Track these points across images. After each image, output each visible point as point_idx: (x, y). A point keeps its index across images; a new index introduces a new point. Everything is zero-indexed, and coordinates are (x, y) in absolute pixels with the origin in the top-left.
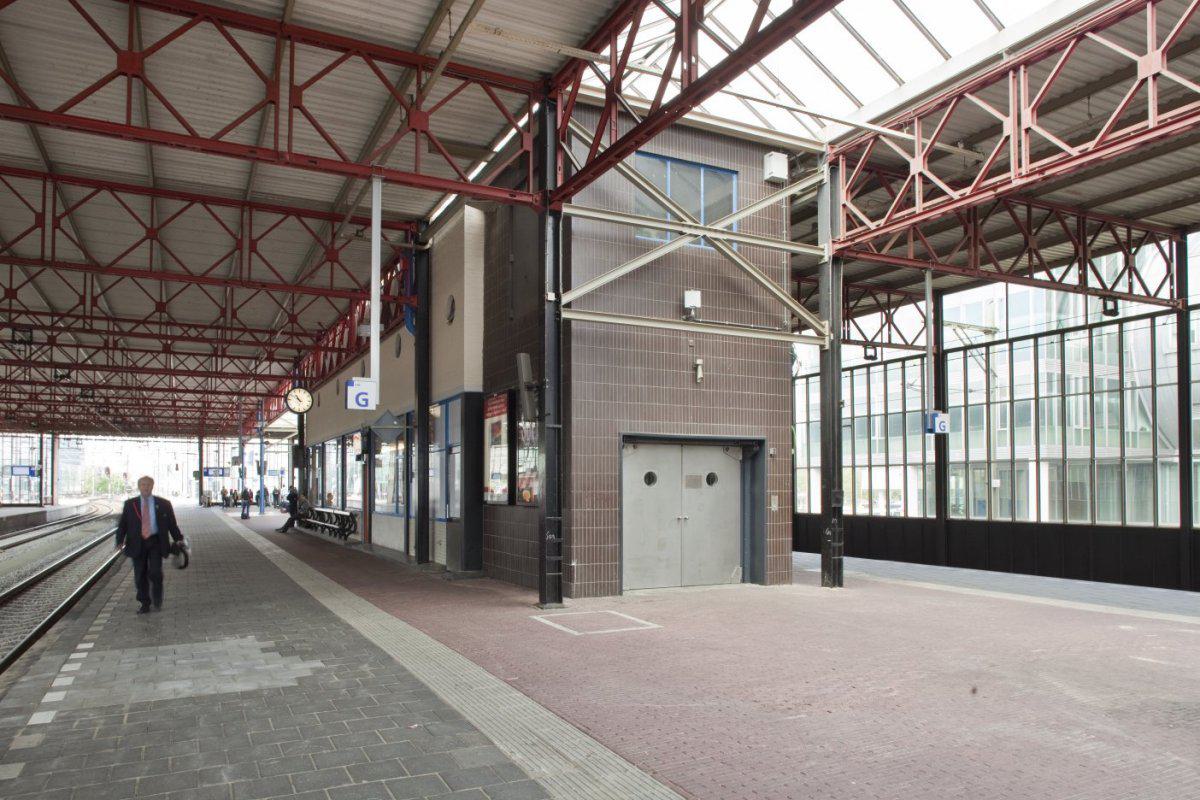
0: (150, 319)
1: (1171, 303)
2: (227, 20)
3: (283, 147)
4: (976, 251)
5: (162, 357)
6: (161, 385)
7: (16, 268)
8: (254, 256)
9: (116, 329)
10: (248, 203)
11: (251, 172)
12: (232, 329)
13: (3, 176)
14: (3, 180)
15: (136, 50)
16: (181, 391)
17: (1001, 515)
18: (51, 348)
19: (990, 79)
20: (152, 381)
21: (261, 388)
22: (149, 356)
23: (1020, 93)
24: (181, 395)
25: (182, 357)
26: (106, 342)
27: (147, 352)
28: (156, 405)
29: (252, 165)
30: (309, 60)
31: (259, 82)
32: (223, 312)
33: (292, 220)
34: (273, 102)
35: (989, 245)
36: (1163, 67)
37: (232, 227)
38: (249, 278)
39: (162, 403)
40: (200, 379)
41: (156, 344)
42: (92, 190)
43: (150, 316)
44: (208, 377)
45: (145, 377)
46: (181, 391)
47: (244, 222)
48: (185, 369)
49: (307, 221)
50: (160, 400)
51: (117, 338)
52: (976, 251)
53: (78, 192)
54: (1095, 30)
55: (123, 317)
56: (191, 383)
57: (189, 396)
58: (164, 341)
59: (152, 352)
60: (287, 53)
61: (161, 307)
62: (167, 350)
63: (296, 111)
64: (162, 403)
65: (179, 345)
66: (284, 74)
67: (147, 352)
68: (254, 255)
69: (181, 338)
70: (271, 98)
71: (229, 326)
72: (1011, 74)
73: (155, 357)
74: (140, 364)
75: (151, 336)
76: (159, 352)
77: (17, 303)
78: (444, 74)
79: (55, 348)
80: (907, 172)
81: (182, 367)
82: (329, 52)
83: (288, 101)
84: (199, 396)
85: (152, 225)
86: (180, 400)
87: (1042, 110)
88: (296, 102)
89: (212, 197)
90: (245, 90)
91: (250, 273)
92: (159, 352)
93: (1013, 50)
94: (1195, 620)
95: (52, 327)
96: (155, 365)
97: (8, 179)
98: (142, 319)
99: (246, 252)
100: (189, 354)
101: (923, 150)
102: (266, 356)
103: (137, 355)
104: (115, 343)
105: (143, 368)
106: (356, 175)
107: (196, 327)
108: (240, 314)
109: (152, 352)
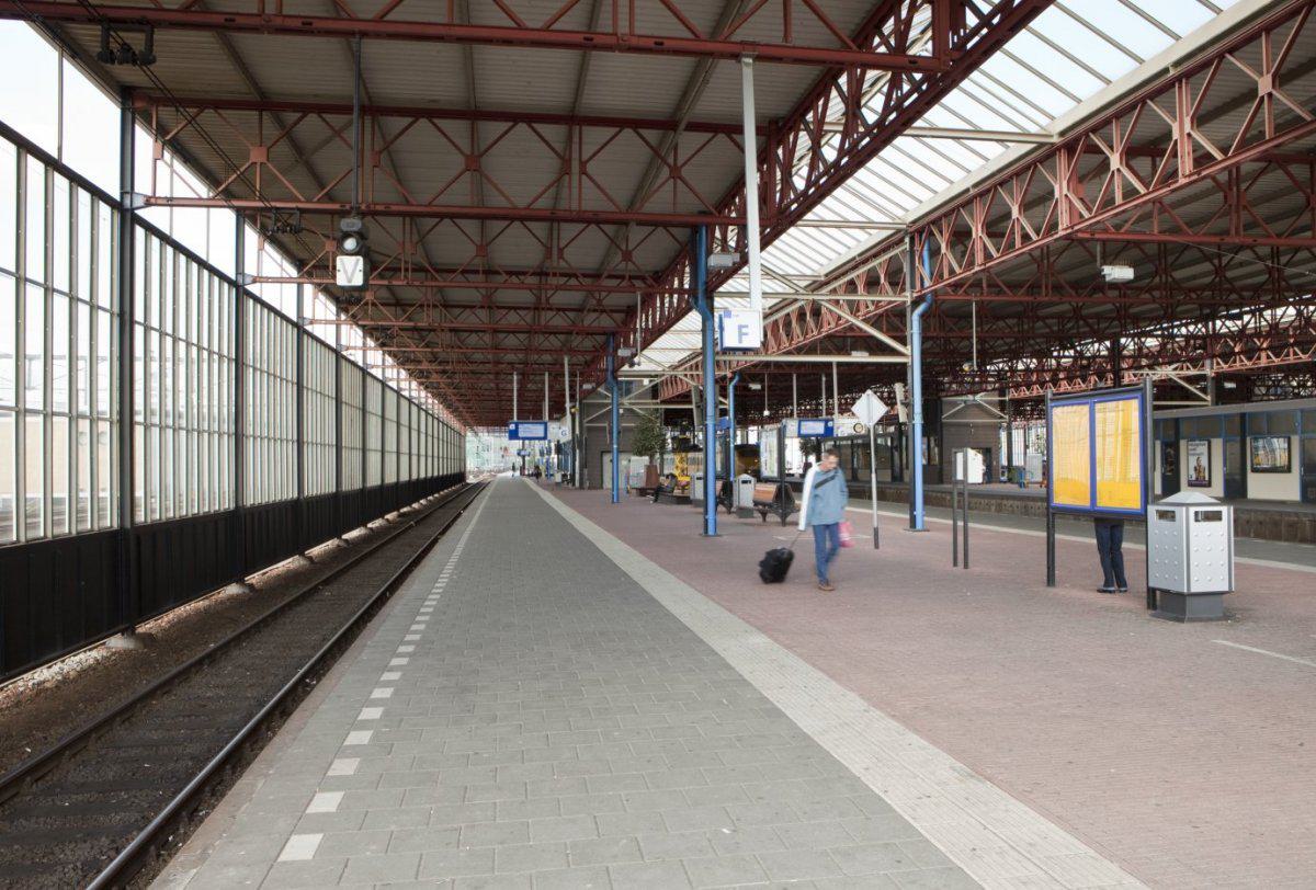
3: (623, 28)
4: (1239, 217)
7: (266, 116)
10: (573, 118)
11: (556, 198)
15: (476, 153)
19: (1158, 88)
21: (588, 343)
23: (1185, 102)
29: (584, 57)
31: (541, 247)
32: (548, 251)
33: (628, 133)
35: (1254, 210)
36: (1121, 163)
37: (559, 147)
47: (578, 146)
49: (645, 132)
52: (1239, 217)
53: (396, 123)
54: (1231, 51)
55: (455, 303)
60: (577, 131)
66: (575, 155)
68: (584, 177)
72: (1177, 85)
80: (1010, 217)
82: (606, 129)
87: (1200, 120)
88: (583, 172)
89: (537, 115)
90: (547, 165)
91: (580, 203)
93: (975, 185)
94: (1313, 570)
99: (575, 178)
101: (1121, 142)
106: (711, 54)
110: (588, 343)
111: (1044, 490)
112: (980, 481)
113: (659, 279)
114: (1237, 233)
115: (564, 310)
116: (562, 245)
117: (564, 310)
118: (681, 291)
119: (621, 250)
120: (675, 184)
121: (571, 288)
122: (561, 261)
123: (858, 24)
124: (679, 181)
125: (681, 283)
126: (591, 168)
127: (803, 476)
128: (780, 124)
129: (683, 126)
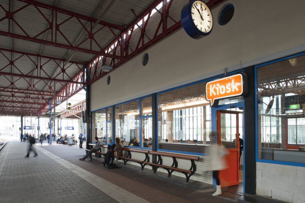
0: (9, 87)
1: (295, 89)
2: (37, 4)
5: (11, 98)
6: (10, 105)
8: (41, 70)
9: (51, 94)
12: (33, 90)
13: (1, 51)
14: (1, 52)
16: (16, 107)
17: (303, 143)
18: (43, 100)
20: (8, 104)
21: (39, 106)
22: (7, 97)
24: (16, 108)
25: (17, 98)
26: (27, 96)
27: (6, 96)
28: (9, 111)
30: (62, 17)
34: (51, 29)
38: (40, 76)
39: (10, 110)
40: (22, 104)
41: (10, 94)
42: (22, 55)
43: (9, 86)
44: (24, 103)
45: (5, 103)
46: (16, 107)
48: (18, 101)
50: (10, 110)
51: (30, 95)
56: (19, 105)
57: (18, 109)
58: (12, 93)
59: (8, 96)
61: (12, 84)
62: (13, 96)
63: (57, 31)
64: (10, 110)
65: (17, 94)
67: (6, 96)
68: (41, 70)
69: (17, 92)
70: (51, 27)
71: (32, 89)
73: (9, 98)
74: (5, 99)
75: (8, 91)
76: (10, 96)
77: (35, 88)
78: (99, 23)
79: (44, 100)
81: (17, 100)
83: (55, 27)
84: (21, 108)
85: (12, 60)
86: (16, 109)
88: (57, 29)
92: (10, 96)
95: (43, 94)
96: (9, 100)
97: (2, 51)
98: (7, 87)
100: (19, 97)
102: (41, 98)
103: (3, 97)
104: (29, 96)
105: (6, 100)
107: (21, 89)
108: (35, 86)
109: (8, 96)
110: (39, 106)
111: (199, 108)
112: (206, 106)
113: (57, 93)
114: (74, 110)
115: (33, 98)
116: (36, 69)
117: (33, 98)
118: (63, 97)
119: (87, 31)
120: (91, 41)
121: (21, 92)
122: (34, 88)
123: (140, 12)
124: (93, 40)
125: (63, 94)
126: (61, 28)
127: (291, 110)
128: (126, 27)
129: (98, 21)
